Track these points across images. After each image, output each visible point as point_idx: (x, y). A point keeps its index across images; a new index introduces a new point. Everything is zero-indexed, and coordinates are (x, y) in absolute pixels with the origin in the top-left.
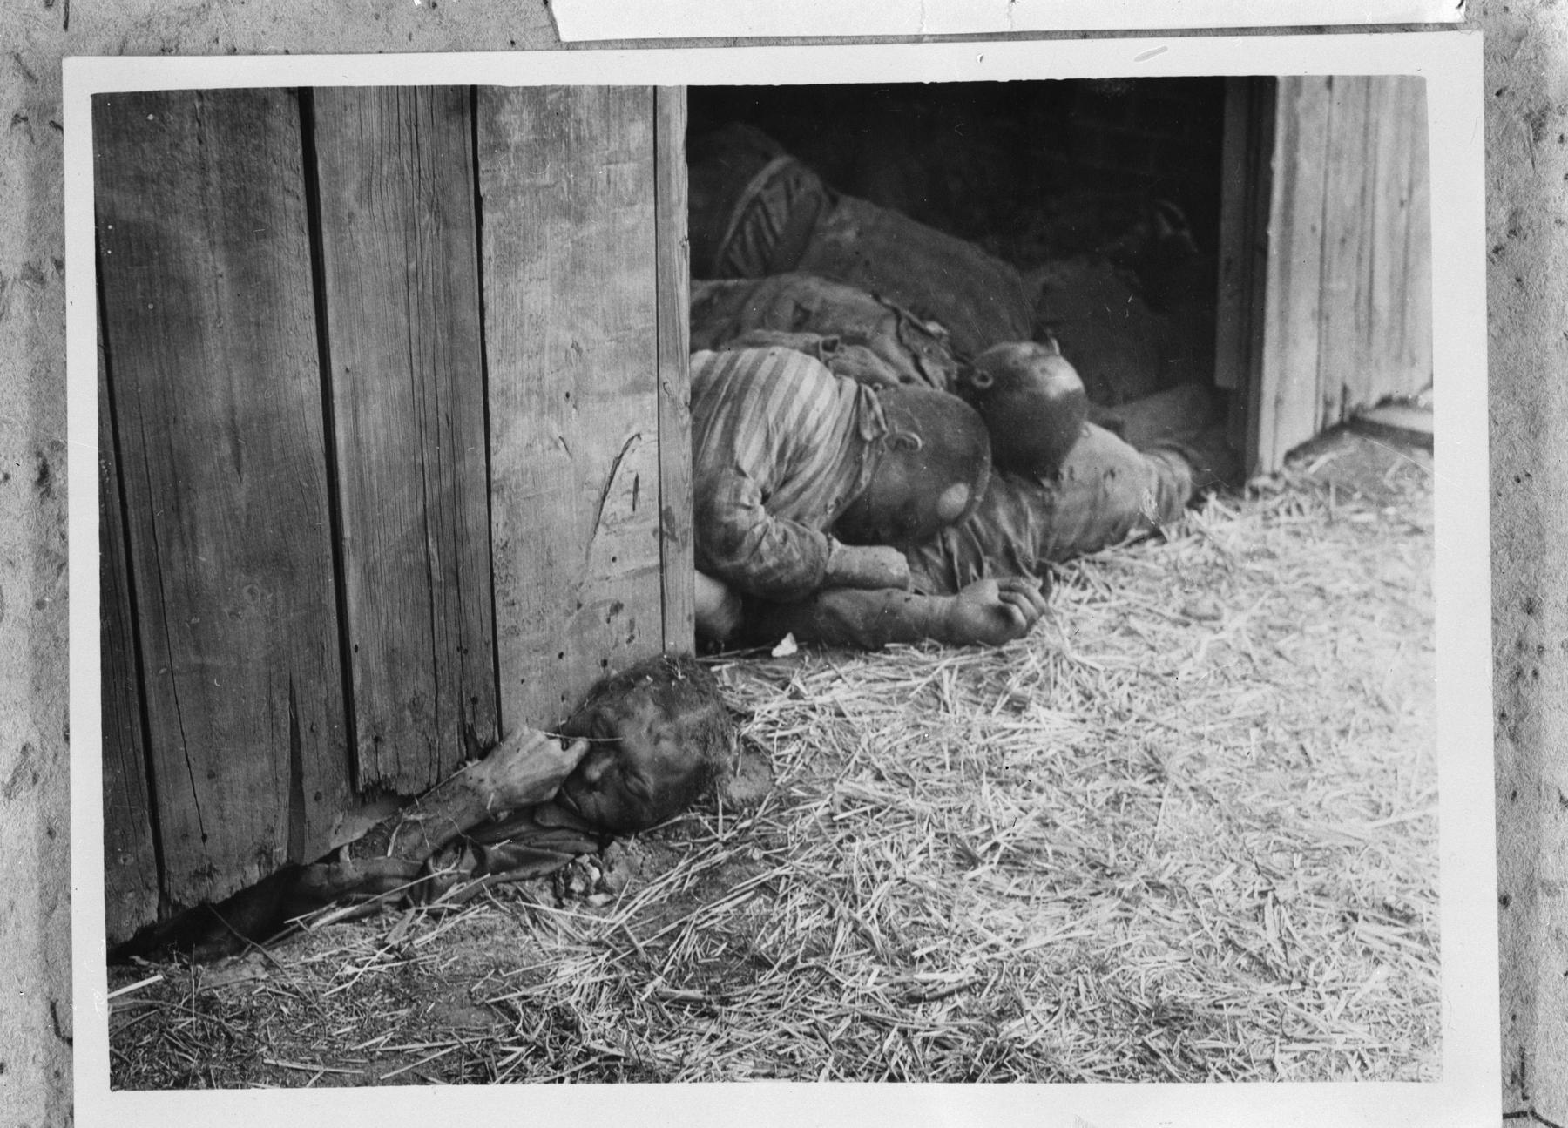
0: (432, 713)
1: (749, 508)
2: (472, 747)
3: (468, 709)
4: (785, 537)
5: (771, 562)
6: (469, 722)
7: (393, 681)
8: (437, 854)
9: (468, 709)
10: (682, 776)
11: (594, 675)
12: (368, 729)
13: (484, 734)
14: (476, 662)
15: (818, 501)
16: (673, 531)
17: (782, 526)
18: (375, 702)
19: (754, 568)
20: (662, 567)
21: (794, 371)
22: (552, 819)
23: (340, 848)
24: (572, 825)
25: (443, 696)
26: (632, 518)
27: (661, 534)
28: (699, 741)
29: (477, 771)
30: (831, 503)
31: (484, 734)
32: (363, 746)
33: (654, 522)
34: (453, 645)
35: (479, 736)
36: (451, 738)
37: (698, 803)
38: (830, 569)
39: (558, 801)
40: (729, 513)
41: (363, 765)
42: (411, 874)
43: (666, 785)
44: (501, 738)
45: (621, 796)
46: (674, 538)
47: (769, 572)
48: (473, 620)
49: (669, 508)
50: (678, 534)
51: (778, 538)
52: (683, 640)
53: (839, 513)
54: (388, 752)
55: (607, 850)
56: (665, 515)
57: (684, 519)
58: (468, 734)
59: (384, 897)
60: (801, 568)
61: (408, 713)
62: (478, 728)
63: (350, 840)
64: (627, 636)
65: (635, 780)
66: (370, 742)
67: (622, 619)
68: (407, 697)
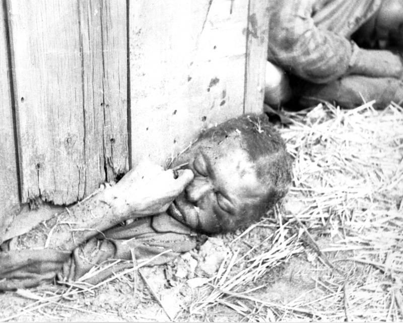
0: (81, 148)
1: (304, 19)
2: (110, 172)
3: (108, 147)
4: (325, 41)
5: (314, 56)
6: (108, 155)
7: (52, 126)
8: (82, 245)
9: (108, 147)
10: (258, 199)
11: (198, 127)
12: (32, 159)
13: (119, 164)
14: (114, 114)
15: (344, 19)
16: (256, 30)
17: (322, 33)
18: (37, 141)
19: (303, 59)
20: (247, 55)
21: (5, 108)
22: (164, 223)
23: (10, 240)
24: (179, 230)
25: (89, 137)
26: (229, 19)
27: (248, 33)
28: (272, 176)
29: (110, 192)
30: (352, 20)
31: (119, 164)
32: (27, 170)
33: (244, 24)
34: (99, 100)
35: (115, 165)
36: (95, 171)
37: (266, 216)
38: (351, 64)
39: (169, 212)
40: (290, 21)
41: (26, 186)
42: (62, 259)
43: (246, 205)
44: (130, 168)
45: (215, 211)
46: (255, 35)
47: (314, 62)
48: (114, 83)
49: (254, 14)
50: (259, 34)
51: (320, 40)
52: (257, 107)
53: (357, 28)
54: (47, 174)
55: (202, 247)
56: (252, 19)
57: (263, 23)
58: (107, 164)
59: (41, 277)
60: (334, 61)
61: (62, 147)
62: (115, 160)
63: (18, 235)
64: (220, 101)
65: (225, 201)
66: (33, 167)
67: (217, 89)
68: (63, 137)
